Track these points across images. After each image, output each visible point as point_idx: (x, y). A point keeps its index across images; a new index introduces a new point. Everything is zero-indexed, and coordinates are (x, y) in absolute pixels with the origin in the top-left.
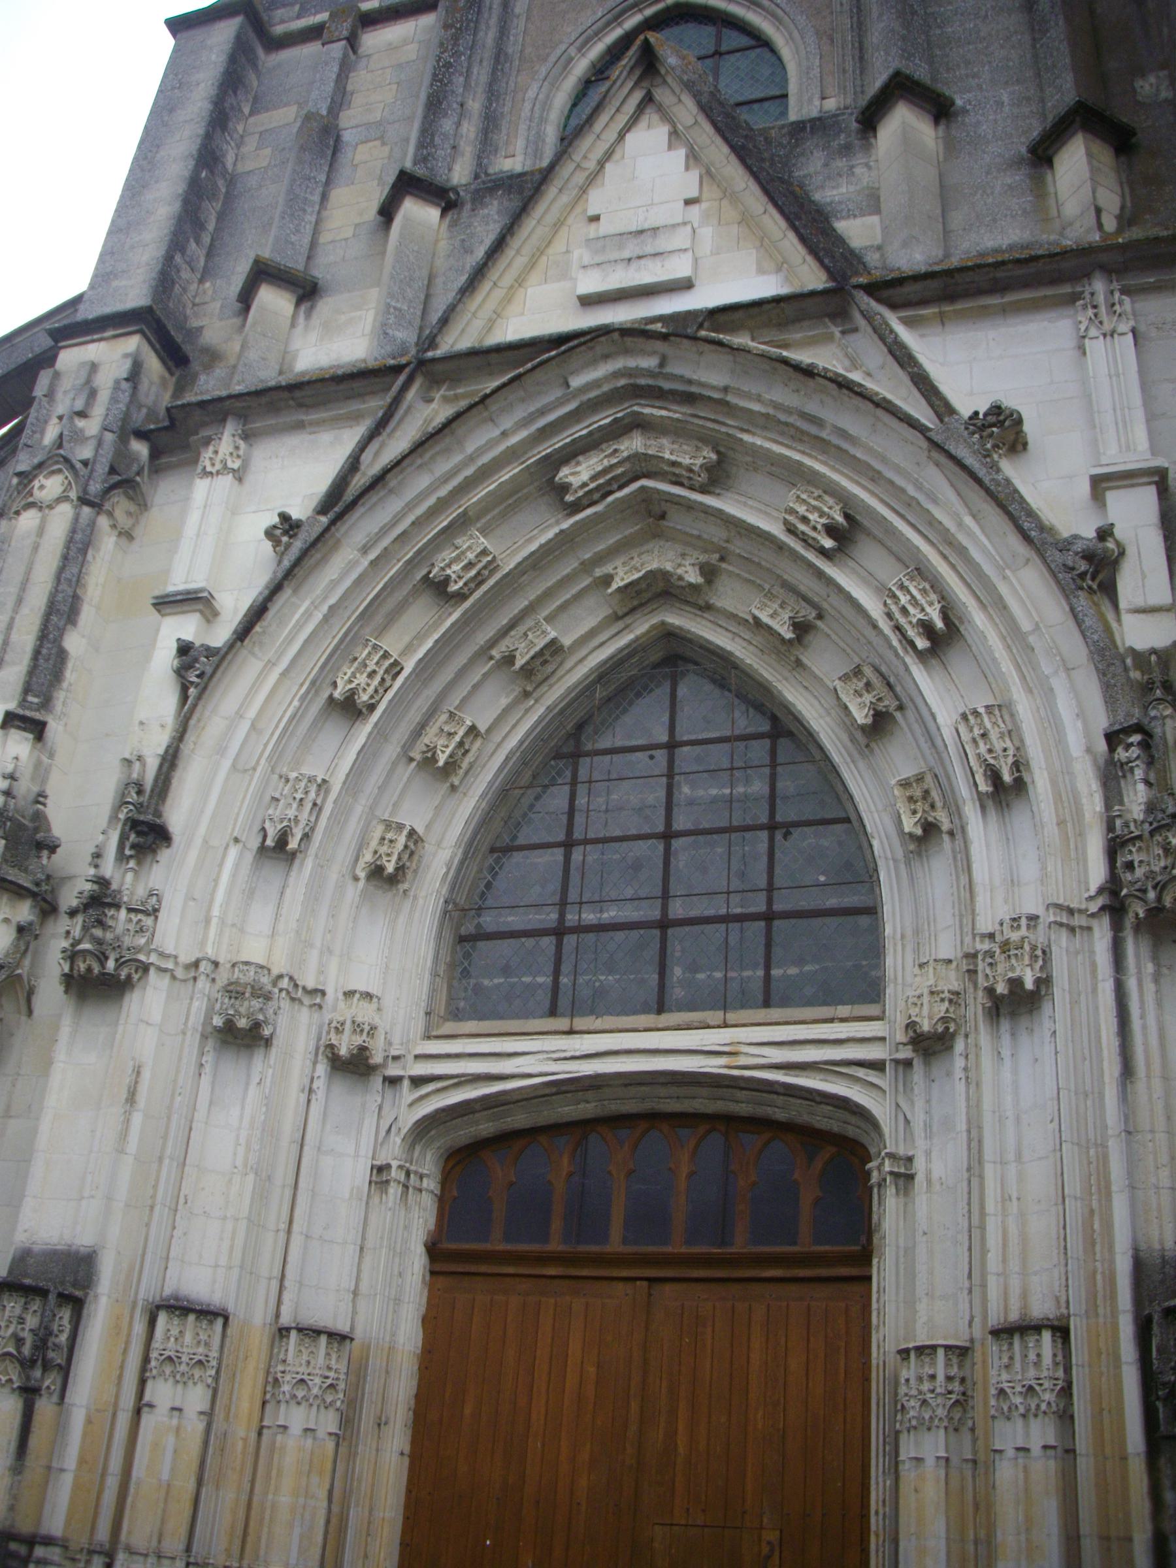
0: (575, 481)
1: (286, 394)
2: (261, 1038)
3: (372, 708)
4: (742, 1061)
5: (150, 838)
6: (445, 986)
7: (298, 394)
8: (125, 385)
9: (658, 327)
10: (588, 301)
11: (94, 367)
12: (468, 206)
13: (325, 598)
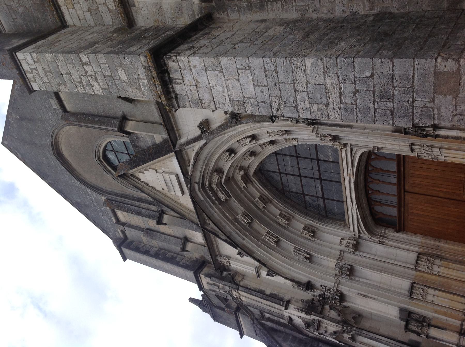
0: (224, 198)
1: (211, 250)
2: (351, 268)
3: (277, 237)
4: (352, 174)
5: (309, 286)
6: (338, 222)
7: (210, 247)
8: (212, 279)
9: (189, 186)
10: (183, 193)
11: (208, 283)
12: (162, 208)
13: (255, 247)
